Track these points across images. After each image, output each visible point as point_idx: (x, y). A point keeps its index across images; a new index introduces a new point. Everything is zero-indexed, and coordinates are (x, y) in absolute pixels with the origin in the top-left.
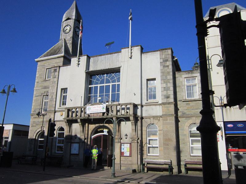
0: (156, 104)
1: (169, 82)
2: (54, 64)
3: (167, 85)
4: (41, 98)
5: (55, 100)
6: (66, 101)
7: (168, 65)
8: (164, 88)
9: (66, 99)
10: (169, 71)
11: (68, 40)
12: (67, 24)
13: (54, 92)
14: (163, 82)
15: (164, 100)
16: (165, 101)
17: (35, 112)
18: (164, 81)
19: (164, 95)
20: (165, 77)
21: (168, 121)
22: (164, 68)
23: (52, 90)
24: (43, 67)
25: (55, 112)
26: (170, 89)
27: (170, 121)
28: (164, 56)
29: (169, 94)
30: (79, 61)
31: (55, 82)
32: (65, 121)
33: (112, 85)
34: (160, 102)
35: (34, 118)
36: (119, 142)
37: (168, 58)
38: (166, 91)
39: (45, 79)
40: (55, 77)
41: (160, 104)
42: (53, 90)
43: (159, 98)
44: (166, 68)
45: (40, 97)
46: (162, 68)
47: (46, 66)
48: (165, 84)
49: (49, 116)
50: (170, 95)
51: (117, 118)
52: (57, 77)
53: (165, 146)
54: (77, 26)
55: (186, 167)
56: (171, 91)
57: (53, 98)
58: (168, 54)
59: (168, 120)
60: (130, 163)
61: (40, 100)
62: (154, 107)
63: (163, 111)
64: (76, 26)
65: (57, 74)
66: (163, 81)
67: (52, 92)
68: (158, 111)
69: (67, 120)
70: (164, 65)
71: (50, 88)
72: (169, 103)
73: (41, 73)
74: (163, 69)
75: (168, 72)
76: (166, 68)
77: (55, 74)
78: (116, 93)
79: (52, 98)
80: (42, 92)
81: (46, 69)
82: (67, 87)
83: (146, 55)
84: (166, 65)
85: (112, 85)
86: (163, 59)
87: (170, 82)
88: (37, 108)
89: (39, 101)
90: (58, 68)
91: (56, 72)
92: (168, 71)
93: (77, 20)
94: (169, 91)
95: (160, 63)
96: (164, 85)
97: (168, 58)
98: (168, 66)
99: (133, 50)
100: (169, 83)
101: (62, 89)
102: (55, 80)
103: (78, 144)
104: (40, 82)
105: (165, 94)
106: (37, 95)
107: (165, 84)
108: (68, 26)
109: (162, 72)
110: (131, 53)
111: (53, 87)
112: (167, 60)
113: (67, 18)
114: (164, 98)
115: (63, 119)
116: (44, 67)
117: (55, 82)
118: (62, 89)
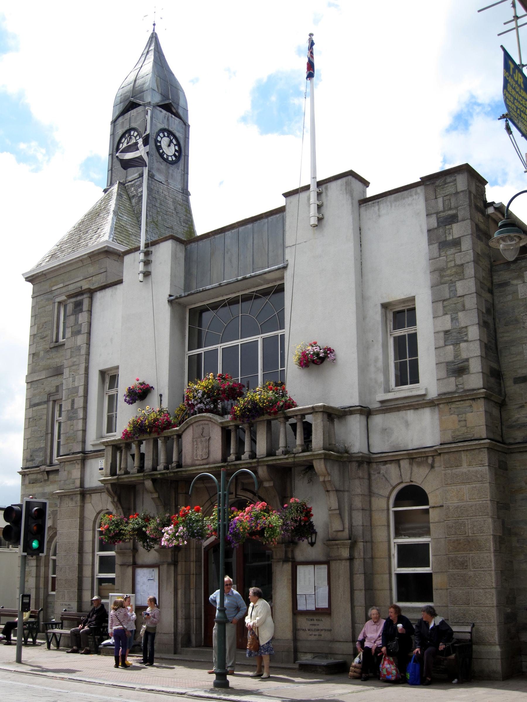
0: (418, 403)
1: (464, 306)
2: (79, 284)
3: (454, 319)
4: (48, 408)
5: (81, 414)
6: (116, 414)
7: (456, 236)
8: (446, 332)
9: (116, 411)
10: (463, 262)
11: (132, 186)
12: (127, 127)
13: (76, 384)
14: (441, 312)
15: (445, 380)
16: (451, 385)
17: (33, 460)
18: (444, 307)
19: (448, 363)
20: (447, 290)
21: (464, 469)
22: (443, 254)
23: (71, 379)
24: (48, 300)
25: (83, 461)
26: (466, 335)
27: (472, 469)
28: (440, 200)
29: (464, 356)
30: (147, 263)
31: (79, 348)
32: (107, 489)
33: (264, 339)
34: (433, 394)
35: (30, 483)
36: (286, 560)
37: (456, 208)
38: (451, 347)
39: (57, 341)
40: (79, 332)
41: (432, 404)
42: (74, 381)
43: (430, 379)
44: (453, 251)
45: (45, 406)
46: (436, 253)
47: (56, 293)
48: (448, 317)
49: (66, 473)
50: (467, 360)
51: (273, 469)
52: (84, 329)
53: (455, 571)
54: (166, 127)
55: (493, 652)
56: (471, 344)
57: (76, 406)
58: (457, 193)
59: (465, 464)
60: (326, 636)
61: (45, 417)
62: (410, 415)
63: (443, 431)
64: (161, 126)
65: (83, 317)
66: (440, 304)
67: (71, 387)
68: (422, 430)
69: (113, 485)
70: (442, 239)
71: (66, 372)
72: (470, 396)
73: (44, 320)
74: (440, 256)
75: (458, 266)
76: (449, 253)
77: (77, 320)
78: (280, 369)
79: (72, 407)
80: (47, 389)
81: (56, 304)
82: (115, 364)
83: (376, 208)
84: (450, 238)
85: (264, 339)
86: (437, 213)
87: (467, 306)
88: (38, 446)
89: (43, 422)
90: (85, 296)
91: (81, 311)
92: (458, 262)
93: (160, 106)
94: (463, 345)
95: (429, 231)
96: (446, 323)
97: (456, 208)
98: (456, 243)
99: (327, 195)
100: (464, 310)
101: (103, 373)
102: (79, 343)
103: (326, 566)
104: (42, 353)
105: (450, 358)
106: (37, 401)
107: (448, 317)
108: (132, 133)
109: (435, 271)
110: (319, 207)
111: (73, 368)
112: (453, 219)
113: (127, 103)
114: (445, 376)
115: (100, 484)
116: (50, 296)
117: (79, 348)
118: (103, 373)
